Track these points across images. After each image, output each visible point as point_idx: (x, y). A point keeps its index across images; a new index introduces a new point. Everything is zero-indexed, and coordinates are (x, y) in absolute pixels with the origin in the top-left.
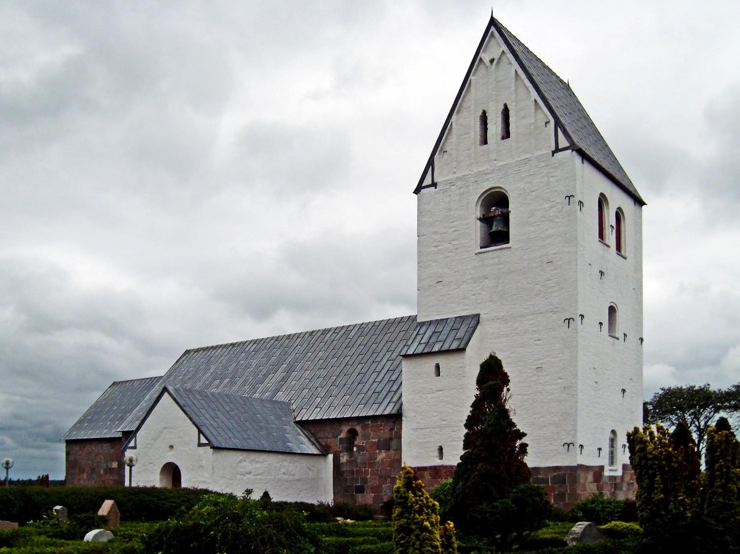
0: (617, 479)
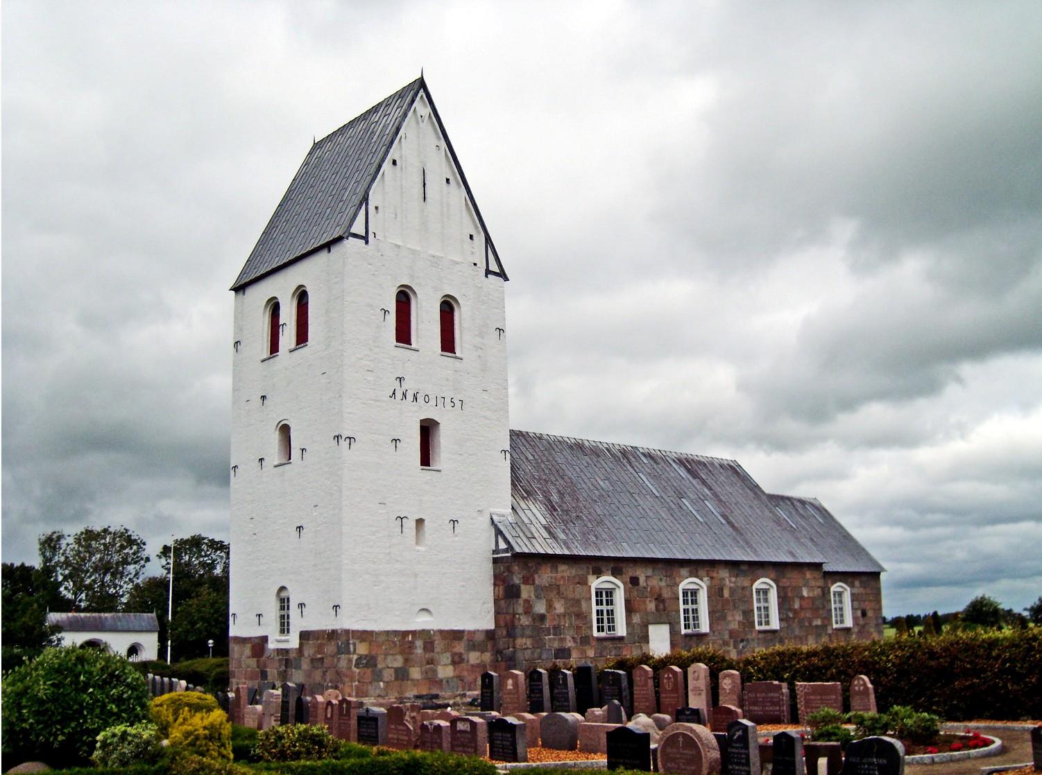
0: (290, 652)
